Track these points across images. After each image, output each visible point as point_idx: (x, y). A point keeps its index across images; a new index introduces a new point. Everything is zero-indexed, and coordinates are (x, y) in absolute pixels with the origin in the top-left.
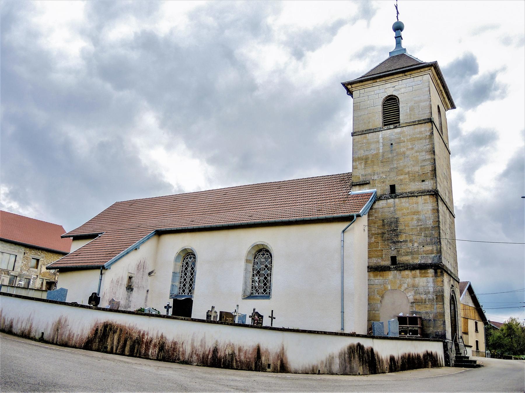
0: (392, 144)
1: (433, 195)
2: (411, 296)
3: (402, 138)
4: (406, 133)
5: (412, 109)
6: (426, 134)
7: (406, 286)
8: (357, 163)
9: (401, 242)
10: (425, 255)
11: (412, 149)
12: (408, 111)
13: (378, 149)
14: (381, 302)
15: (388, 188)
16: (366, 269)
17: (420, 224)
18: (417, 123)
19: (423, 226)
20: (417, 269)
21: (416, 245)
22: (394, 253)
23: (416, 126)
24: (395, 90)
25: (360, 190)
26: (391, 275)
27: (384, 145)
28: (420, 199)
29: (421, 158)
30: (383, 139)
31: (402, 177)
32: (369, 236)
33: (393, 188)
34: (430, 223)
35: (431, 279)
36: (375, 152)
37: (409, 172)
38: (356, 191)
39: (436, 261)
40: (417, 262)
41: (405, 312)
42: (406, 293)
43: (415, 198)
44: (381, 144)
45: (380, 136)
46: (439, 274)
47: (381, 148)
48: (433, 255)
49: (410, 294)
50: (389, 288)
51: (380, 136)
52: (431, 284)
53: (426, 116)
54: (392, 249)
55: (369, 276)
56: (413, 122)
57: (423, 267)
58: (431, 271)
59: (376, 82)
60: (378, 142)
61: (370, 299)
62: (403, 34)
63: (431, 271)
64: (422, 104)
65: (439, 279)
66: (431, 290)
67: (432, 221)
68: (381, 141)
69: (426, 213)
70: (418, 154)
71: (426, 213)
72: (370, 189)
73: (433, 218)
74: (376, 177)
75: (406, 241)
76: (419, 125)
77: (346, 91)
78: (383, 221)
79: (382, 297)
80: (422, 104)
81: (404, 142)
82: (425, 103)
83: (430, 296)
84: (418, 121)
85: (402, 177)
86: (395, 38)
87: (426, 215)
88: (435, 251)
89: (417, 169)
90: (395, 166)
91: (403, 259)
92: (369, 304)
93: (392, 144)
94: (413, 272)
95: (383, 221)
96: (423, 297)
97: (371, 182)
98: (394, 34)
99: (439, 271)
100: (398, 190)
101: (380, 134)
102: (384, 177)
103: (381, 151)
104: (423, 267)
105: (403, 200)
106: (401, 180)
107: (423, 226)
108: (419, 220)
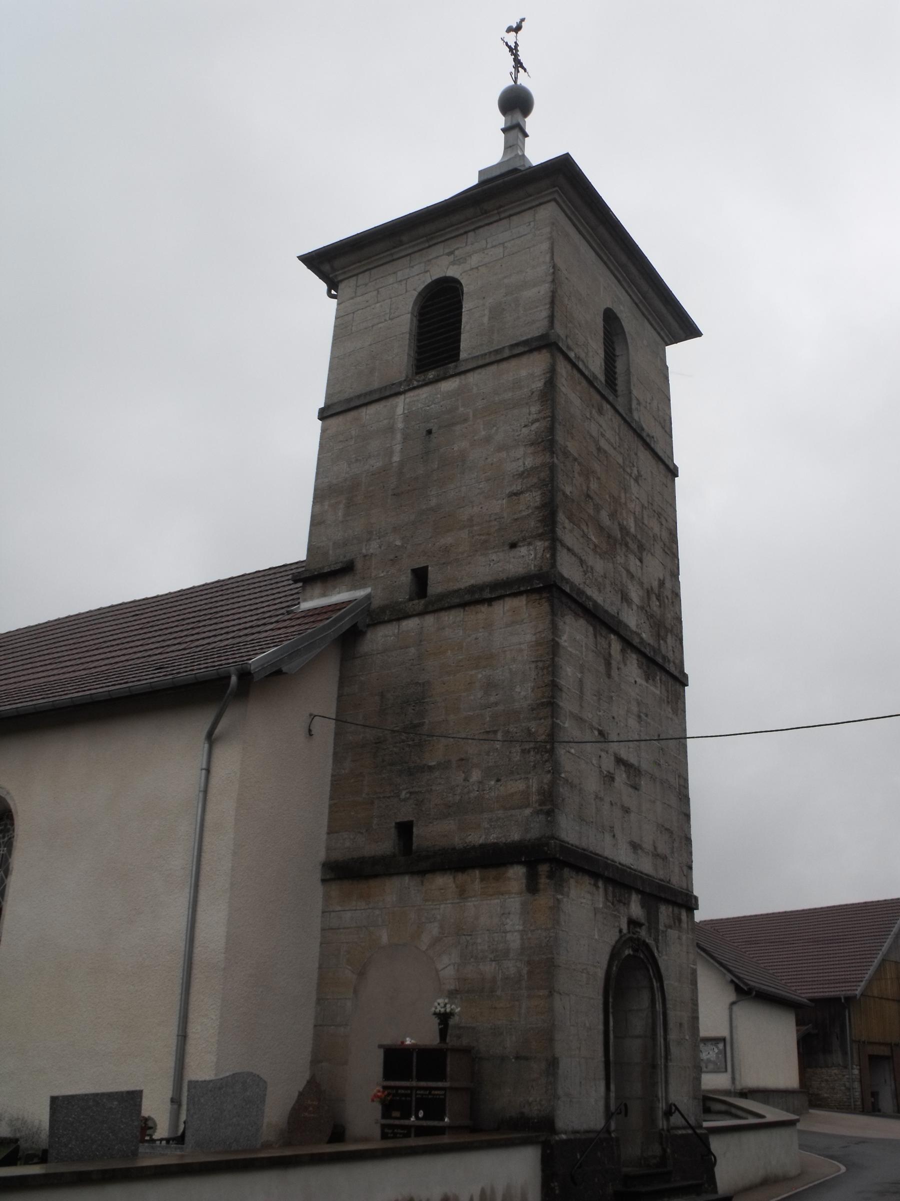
0: (429, 432)
1: (538, 591)
2: (447, 967)
3: (461, 409)
4: (475, 390)
5: (497, 312)
6: (534, 386)
7: (434, 929)
8: (326, 503)
9: (431, 769)
10: (500, 813)
11: (488, 440)
12: (486, 320)
13: (390, 453)
14: (355, 992)
15: (406, 579)
16: (318, 875)
17: (492, 699)
18: (507, 353)
19: (501, 708)
20: (473, 867)
21: (476, 775)
22: (405, 813)
23: (504, 366)
24: (453, 263)
25: (324, 595)
26: (393, 892)
27: (406, 438)
28: (501, 611)
29: (512, 467)
30: (407, 417)
31: (448, 540)
32: (335, 754)
33: (420, 576)
34: (525, 693)
35: (514, 903)
36: (379, 464)
37: (471, 519)
38: (312, 598)
39: (536, 831)
40: (476, 838)
41: (419, 1034)
42: (446, 953)
43: (484, 608)
44: (399, 436)
45: (400, 410)
46: (543, 880)
47: (398, 448)
48: (528, 811)
49: (445, 960)
50: (385, 939)
51: (400, 410)
52: (514, 923)
53: (533, 324)
54: (403, 795)
55: (327, 898)
56: (497, 352)
57: (489, 859)
58: (517, 873)
59: (401, 243)
60: (391, 429)
61: (325, 980)
62: (531, 123)
63: (517, 873)
64: (529, 294)
65: (544, 900)
66: (514, 941)
67: (531, 684)
68: (400, 425)
69: (514, 660)
70: (504, 454)
71: (514, 660)
72: (354, 587)
73: (533, 674)
74: (373, 547)
75: (445, 766)
76: (513, 363)
77: (324, 286)
78: (382, 695)
79: (362, 974)
80: (529, 294)
81: (466, 420)
82: (535, 290)
83: (511, 967)
84: (512, 346)
85: (448, 540)
86: (504, 130)
87: (514, 667)
88: (534, 798)
89: (497, 506)
90: (433, 502)
91: (432, 833)
92: (319, 1001)
93: (429, 432)
94: (461, 877)
95: (382, 695)
96: (489, 968)
97: (359, 565)
98: (500, 121)
99: (544, 869)
100: (437, 584)
101: (400, 405)
102: (398, 543)
103: (396, 458)
104: (489, 859)
105: (449, 618)
106: (446, 550)
107: (501, 708)
108: (490, 686)
